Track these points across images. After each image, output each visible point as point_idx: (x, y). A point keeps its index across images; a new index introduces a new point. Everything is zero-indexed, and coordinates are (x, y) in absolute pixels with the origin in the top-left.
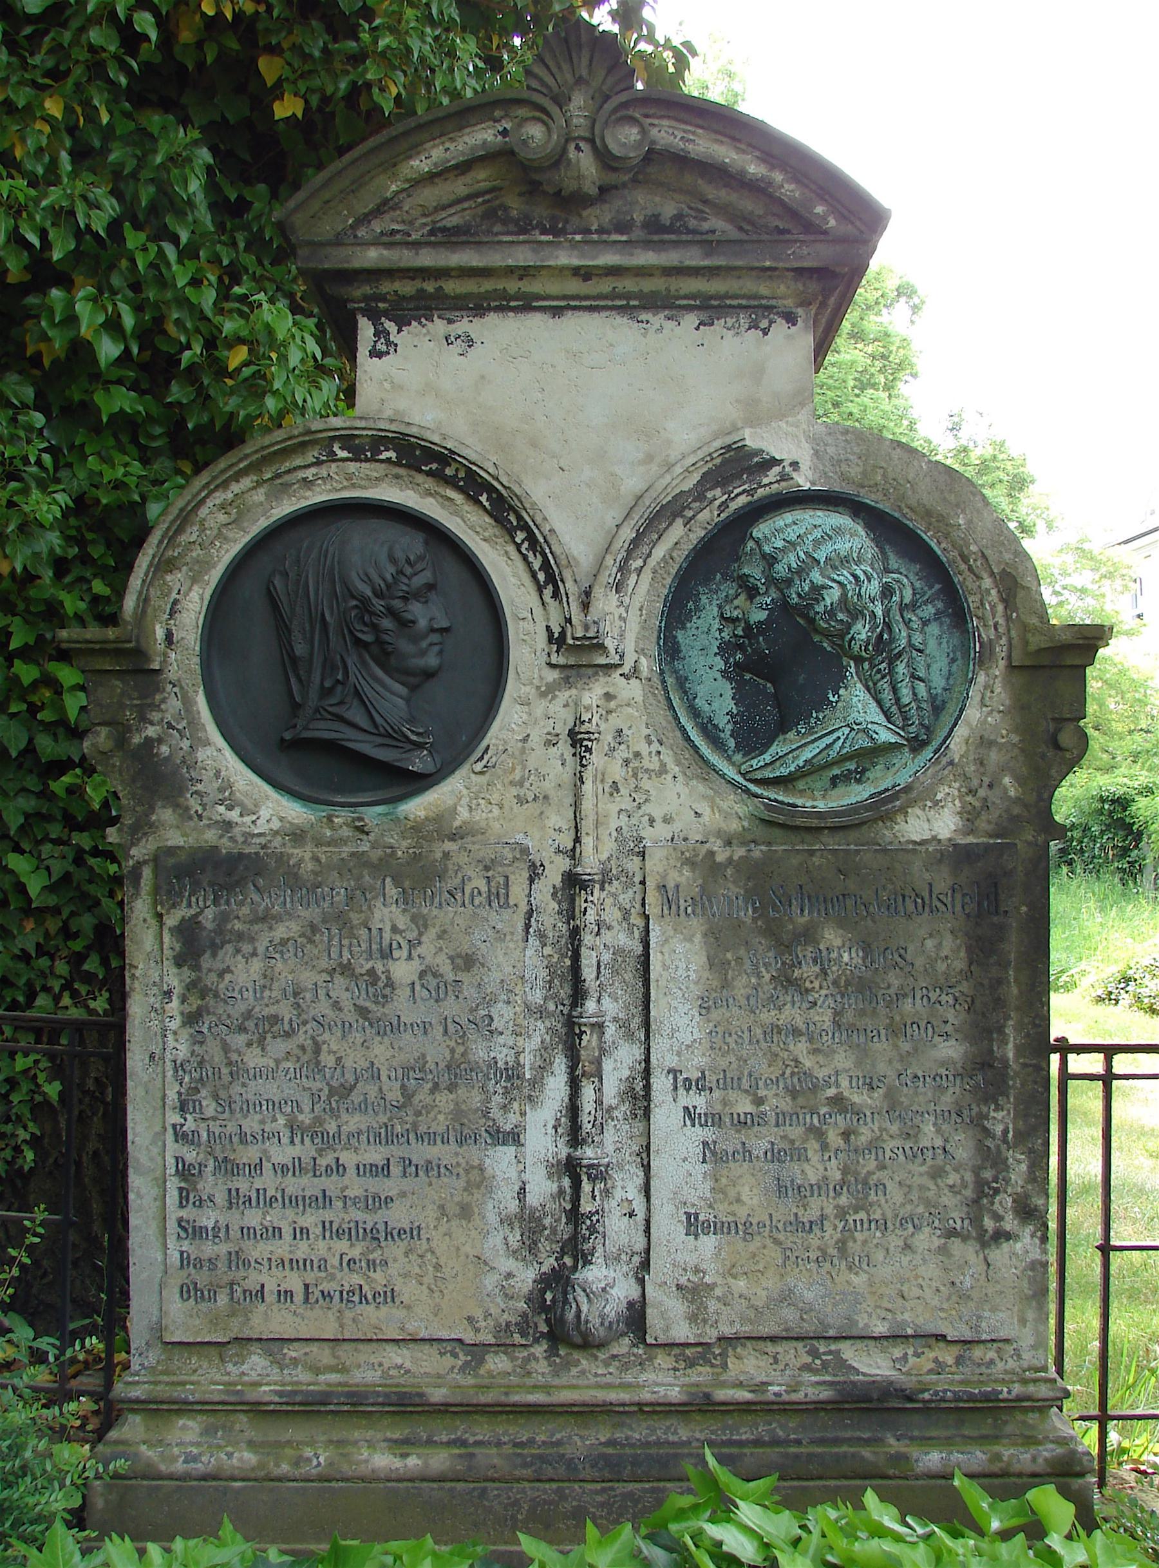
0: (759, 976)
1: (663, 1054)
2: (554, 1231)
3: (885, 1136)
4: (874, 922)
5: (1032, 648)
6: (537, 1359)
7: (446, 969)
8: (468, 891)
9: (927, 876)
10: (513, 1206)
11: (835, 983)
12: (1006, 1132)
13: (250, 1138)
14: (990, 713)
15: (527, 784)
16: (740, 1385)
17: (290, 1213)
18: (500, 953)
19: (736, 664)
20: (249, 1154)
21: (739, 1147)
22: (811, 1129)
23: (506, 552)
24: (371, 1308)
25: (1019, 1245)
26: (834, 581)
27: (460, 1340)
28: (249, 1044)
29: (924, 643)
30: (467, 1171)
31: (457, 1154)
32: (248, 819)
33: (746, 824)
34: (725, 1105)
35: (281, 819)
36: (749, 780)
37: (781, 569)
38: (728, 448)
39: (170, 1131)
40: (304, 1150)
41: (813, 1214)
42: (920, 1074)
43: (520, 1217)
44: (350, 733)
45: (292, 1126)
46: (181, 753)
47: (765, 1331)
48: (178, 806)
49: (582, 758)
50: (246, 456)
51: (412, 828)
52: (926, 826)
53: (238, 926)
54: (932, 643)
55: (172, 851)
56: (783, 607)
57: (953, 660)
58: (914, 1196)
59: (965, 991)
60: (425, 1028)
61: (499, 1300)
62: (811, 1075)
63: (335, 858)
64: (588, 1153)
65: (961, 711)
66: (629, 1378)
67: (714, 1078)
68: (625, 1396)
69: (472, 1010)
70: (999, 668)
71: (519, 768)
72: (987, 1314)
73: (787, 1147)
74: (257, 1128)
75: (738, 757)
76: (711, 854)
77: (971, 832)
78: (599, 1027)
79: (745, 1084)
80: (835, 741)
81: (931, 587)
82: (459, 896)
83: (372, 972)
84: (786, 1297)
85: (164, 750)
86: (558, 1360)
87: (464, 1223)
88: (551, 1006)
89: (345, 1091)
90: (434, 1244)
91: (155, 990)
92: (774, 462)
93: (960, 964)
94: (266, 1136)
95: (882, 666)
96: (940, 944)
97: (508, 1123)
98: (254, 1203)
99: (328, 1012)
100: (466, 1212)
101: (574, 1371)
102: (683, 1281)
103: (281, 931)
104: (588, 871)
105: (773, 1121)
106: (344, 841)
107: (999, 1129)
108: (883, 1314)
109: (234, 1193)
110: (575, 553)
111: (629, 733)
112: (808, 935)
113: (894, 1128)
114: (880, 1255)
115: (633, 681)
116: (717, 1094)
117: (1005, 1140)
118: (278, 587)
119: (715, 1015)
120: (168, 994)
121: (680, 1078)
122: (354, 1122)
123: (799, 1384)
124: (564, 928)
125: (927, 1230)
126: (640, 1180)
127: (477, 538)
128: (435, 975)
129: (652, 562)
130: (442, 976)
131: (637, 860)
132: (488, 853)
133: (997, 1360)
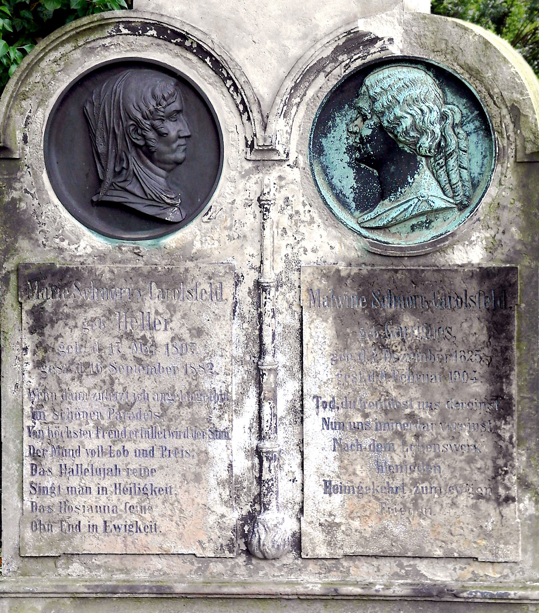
0: (366, 343)
1: (310, 388)
2: (249, 490)
3: (439, 438)
4: (432, 312)
5: (528, 152)
6: (239, 566)
7: (186, 335)
8: (199, 291)
9: (464, 286)
10: (225, 475)
11: (410, 347)
12: (511, 437)
13: (73, 434)
14: (504, 190)
15: (234, 229)
16: (356, 584)
17: (96, 479)
18: (217, 327)
19: (356, 159)
20: (73, 444)
21: (354, 442)
22: (397, 433)
23: (222, 92)
24: (143, 535)
25: (521, 505)
26: (408, 113)
27: (194, 554)
28: (73, 379)
29: (467, 146)
30: (198, 455)
31: (192, 444)
32: (73, 247)
33: (359, 254)
34: (346, 417)
35: (92, 247)
36: (363, 227)
37: (378, 106)
38: (349, 33)
39: (26, 430)
40: (105, 441)
41: (398, 483)
42: (460, 402)
43: (229, 481)
44: (131, 198)
45: (97, 427)
46: (33, 208)
47: (371, 552)
48: (31, 238)
49: (264, 214)
50: (66, 33)
51: (168, 253)
52: (465, 255)
53: (66, 310)
54: (472, 147)
55: (27, 266)
56: (380, 128)
57: (485, 157)
58: (457, 474)
59: (487, 354)
60: (175, 370)
61: (216, 530)
62: (396, 401)
63: (123, 271)
64: (267, 445)
65: (487, 188)
66: (292, 578)
67: (340, 402)
68: (288, 590)
69: (202, 360)
70: (510, 163)
71: (229, 219)
72: (502, 546)
73: (382, 443)
74: (77, 428)
75: (357, 213)
76: (338, 271)
77: (492, 259)
78: (275, 371)
79: (358, 406)
80: (409, 207)
81: (472, 113)
82: (194, 294)
83: (144, 337)
84: (383, 532)
85: (23, 205)
86: (252, 567)
87: (196, 485)
88: (248, 358)
89: (128, 407)
90: (179, 497)
91: (18, 347)
92: (376, 39)
93: (484, 337)
94: (82, 433)
95: (440, 161)
96: (471, 326)
97: (222, 425)
98: (75, 472)
99: (119, 360)
100: (198, 478)
101: (261, 573)
102: (322, 521)
103: (91, 313)
104: (267, 281)
105: (374, 428)
106: (129, 261)
107: (507, 436)
108: (440, 544)
109: (63, 467)
110: (261, 92)
111: (293, 199)
112: (394, 319)
113: (445, 433)
114: (437, 508)
115: (295, 169)
116: (341, 411)
117: (511, 443)
118: (88, 111)
119: (340, 365)
120: (25, 349)
121: (320, 401)
122: (133, 425)
123: (391, 584)
124: (255, 313)
125: (465, 494)
126: (299, 461)
127: (206, 83)
128: (180, 340)
129: (306, 99)
130: (183, 340)
131: (297, 273)
132: (210, 269)
133: (510, 574)
